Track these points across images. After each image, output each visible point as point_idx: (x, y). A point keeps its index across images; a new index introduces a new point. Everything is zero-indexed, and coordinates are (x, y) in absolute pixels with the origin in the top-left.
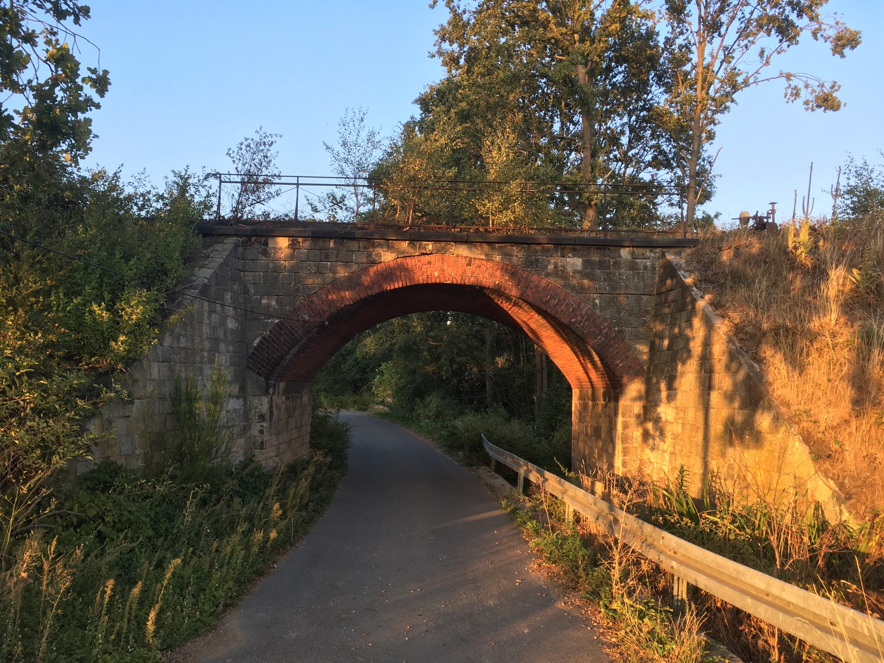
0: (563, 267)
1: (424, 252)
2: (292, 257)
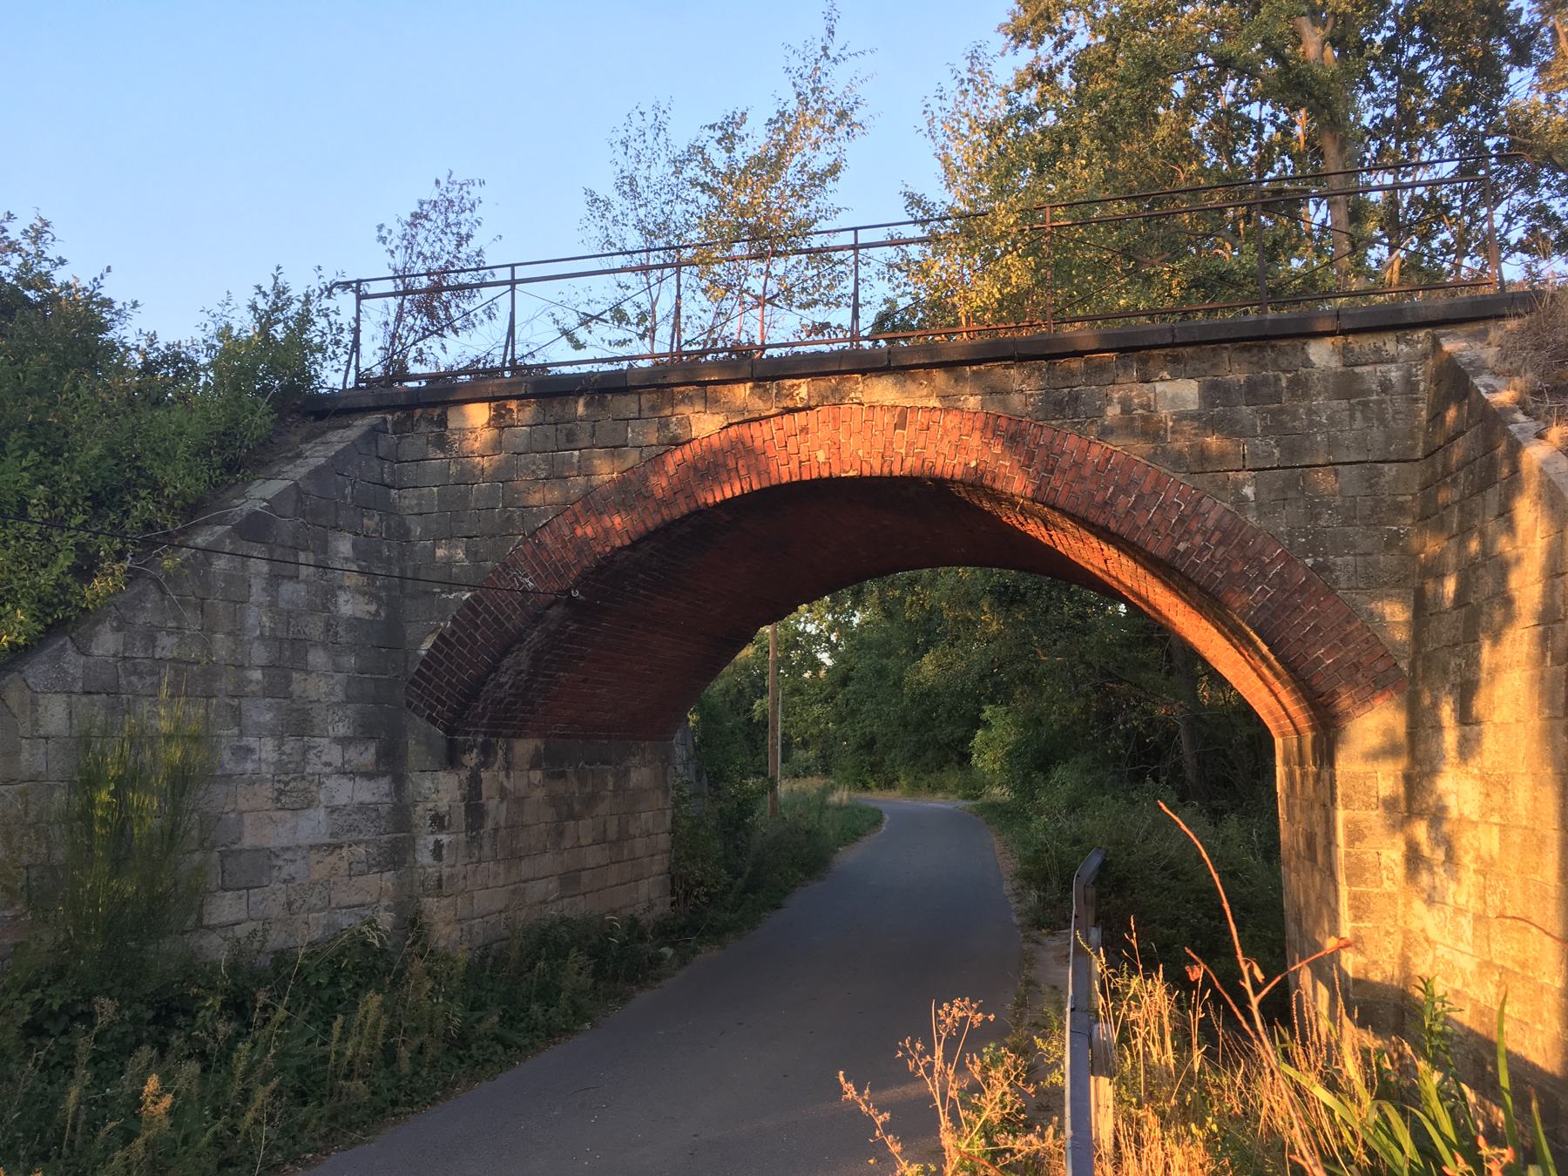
0: (1146, 407)
1: (790, 404)
2: (497, 445)
